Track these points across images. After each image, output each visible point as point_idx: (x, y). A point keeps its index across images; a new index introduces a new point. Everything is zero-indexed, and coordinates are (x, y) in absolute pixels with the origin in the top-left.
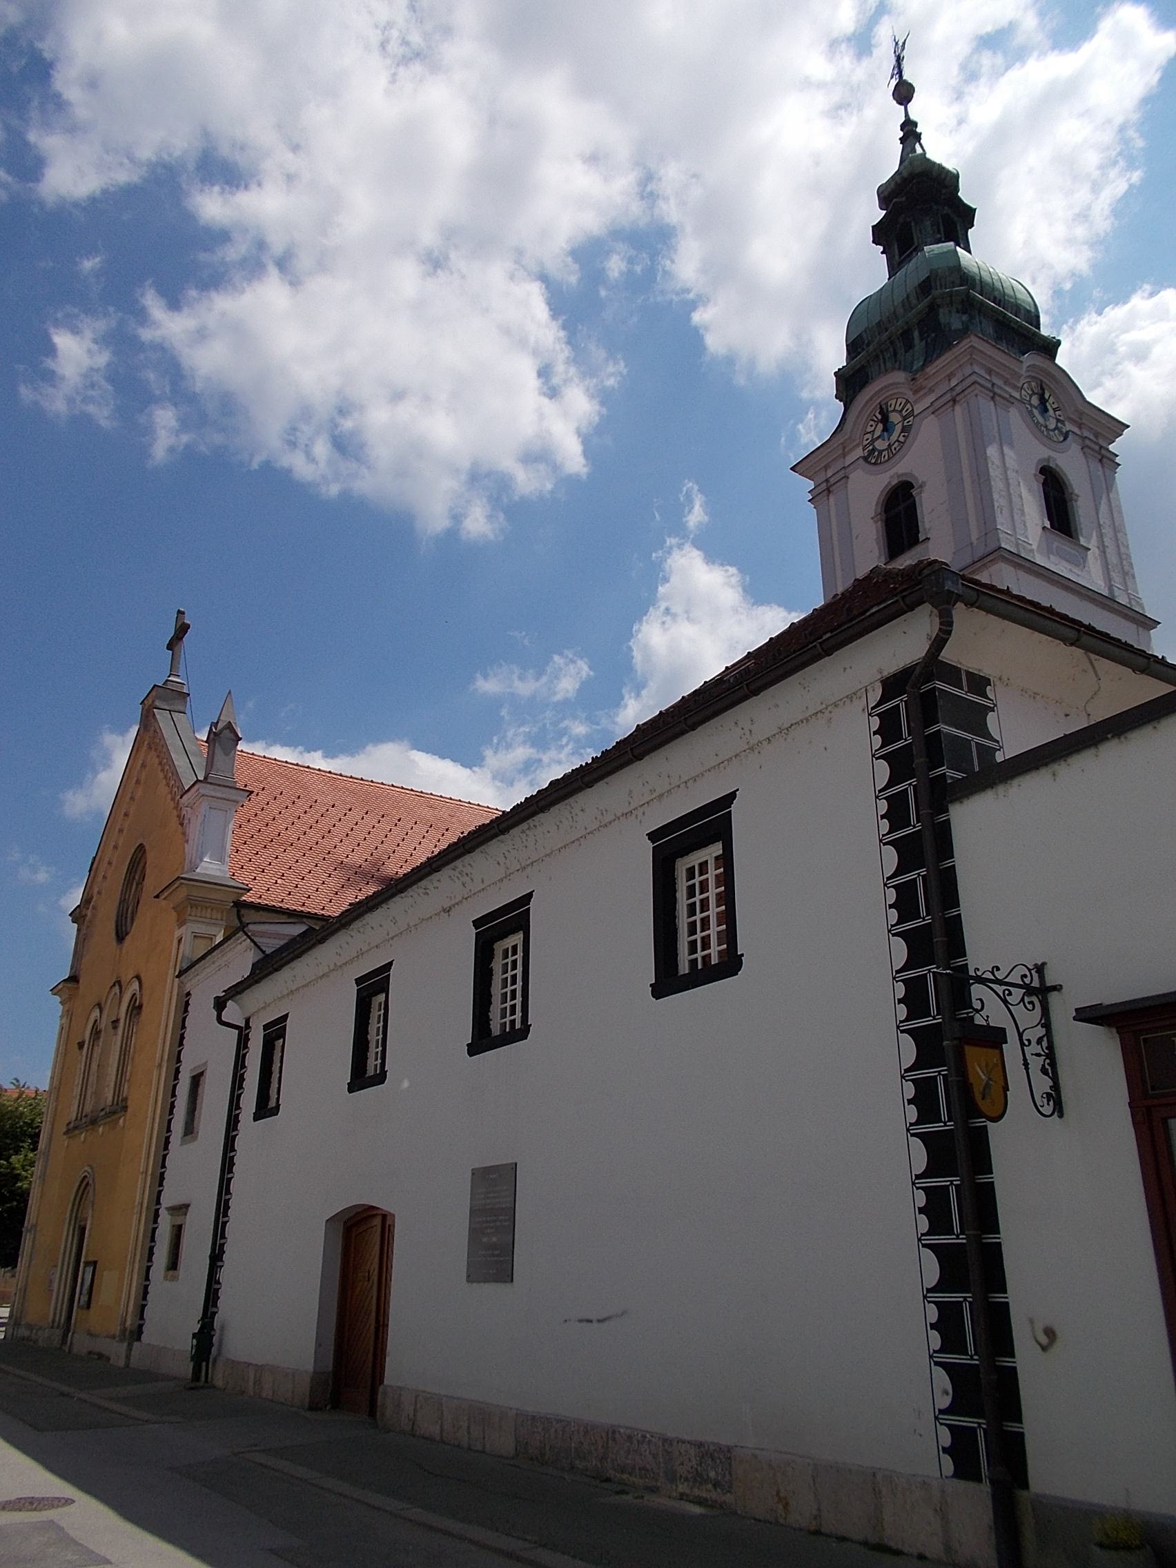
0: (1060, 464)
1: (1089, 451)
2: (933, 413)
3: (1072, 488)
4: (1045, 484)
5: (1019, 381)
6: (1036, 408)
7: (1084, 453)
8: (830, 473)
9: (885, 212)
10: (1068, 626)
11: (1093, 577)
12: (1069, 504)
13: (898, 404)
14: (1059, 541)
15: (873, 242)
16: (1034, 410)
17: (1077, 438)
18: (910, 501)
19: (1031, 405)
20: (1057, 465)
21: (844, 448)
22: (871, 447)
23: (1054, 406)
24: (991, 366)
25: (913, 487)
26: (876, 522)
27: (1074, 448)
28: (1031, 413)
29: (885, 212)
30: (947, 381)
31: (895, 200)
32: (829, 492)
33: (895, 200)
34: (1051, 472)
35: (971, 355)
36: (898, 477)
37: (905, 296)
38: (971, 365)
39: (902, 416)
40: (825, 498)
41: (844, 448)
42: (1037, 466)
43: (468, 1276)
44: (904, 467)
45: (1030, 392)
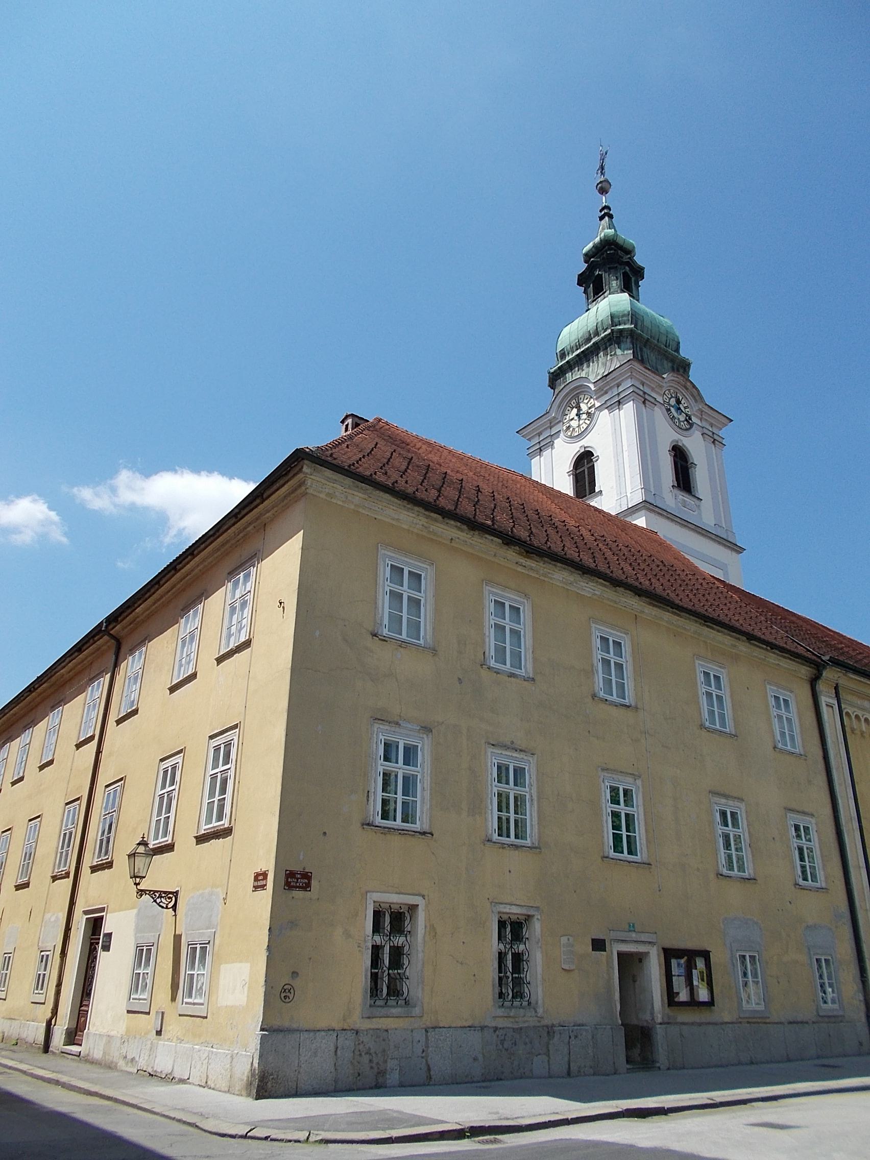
0: (685, 443)
1: (707, 436)
2: (606, 408)
3: (692, 458)
4: (675, 456)
5: (661, 390)
6: (673, 407)
7: (704, 438)
8: (621, 389)
9: (587, 265)
10: (56, 860)
11: (707, 519)
12: (690, 470)
13: (586, 398)
14: (682, 496)
15: (578, 284)
16: (671, 408)
17: (699, 428)
18: (591, 465)
19: (669, 405)
20: (683, 444)
21: (551, 423)
22: (568, 425)
23: (685, 405)
24: (644, 380)
25: (593, 455)
26: (569, 476)
27: (696, 434)
28: (668, 410)
29: (587, 265)
30: (616, 388)
31: (592, 259)
32: (541, 450)
33: (592, 259)
34: (679, 449)
35: (631, 373)
36: (585, 448)
37: (568, 343)
38: (631, 378)
39: (587, 406)
40: (617, 407)
41: (551, 423)
42: (670, 445)
43: (627, 1060)
44: (588, 442)
45: (670, 396)
